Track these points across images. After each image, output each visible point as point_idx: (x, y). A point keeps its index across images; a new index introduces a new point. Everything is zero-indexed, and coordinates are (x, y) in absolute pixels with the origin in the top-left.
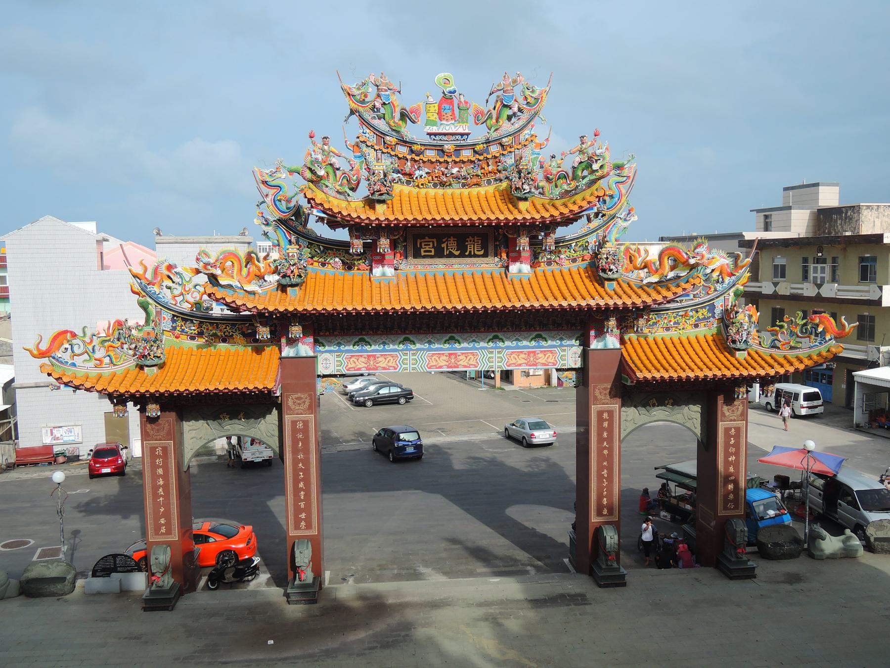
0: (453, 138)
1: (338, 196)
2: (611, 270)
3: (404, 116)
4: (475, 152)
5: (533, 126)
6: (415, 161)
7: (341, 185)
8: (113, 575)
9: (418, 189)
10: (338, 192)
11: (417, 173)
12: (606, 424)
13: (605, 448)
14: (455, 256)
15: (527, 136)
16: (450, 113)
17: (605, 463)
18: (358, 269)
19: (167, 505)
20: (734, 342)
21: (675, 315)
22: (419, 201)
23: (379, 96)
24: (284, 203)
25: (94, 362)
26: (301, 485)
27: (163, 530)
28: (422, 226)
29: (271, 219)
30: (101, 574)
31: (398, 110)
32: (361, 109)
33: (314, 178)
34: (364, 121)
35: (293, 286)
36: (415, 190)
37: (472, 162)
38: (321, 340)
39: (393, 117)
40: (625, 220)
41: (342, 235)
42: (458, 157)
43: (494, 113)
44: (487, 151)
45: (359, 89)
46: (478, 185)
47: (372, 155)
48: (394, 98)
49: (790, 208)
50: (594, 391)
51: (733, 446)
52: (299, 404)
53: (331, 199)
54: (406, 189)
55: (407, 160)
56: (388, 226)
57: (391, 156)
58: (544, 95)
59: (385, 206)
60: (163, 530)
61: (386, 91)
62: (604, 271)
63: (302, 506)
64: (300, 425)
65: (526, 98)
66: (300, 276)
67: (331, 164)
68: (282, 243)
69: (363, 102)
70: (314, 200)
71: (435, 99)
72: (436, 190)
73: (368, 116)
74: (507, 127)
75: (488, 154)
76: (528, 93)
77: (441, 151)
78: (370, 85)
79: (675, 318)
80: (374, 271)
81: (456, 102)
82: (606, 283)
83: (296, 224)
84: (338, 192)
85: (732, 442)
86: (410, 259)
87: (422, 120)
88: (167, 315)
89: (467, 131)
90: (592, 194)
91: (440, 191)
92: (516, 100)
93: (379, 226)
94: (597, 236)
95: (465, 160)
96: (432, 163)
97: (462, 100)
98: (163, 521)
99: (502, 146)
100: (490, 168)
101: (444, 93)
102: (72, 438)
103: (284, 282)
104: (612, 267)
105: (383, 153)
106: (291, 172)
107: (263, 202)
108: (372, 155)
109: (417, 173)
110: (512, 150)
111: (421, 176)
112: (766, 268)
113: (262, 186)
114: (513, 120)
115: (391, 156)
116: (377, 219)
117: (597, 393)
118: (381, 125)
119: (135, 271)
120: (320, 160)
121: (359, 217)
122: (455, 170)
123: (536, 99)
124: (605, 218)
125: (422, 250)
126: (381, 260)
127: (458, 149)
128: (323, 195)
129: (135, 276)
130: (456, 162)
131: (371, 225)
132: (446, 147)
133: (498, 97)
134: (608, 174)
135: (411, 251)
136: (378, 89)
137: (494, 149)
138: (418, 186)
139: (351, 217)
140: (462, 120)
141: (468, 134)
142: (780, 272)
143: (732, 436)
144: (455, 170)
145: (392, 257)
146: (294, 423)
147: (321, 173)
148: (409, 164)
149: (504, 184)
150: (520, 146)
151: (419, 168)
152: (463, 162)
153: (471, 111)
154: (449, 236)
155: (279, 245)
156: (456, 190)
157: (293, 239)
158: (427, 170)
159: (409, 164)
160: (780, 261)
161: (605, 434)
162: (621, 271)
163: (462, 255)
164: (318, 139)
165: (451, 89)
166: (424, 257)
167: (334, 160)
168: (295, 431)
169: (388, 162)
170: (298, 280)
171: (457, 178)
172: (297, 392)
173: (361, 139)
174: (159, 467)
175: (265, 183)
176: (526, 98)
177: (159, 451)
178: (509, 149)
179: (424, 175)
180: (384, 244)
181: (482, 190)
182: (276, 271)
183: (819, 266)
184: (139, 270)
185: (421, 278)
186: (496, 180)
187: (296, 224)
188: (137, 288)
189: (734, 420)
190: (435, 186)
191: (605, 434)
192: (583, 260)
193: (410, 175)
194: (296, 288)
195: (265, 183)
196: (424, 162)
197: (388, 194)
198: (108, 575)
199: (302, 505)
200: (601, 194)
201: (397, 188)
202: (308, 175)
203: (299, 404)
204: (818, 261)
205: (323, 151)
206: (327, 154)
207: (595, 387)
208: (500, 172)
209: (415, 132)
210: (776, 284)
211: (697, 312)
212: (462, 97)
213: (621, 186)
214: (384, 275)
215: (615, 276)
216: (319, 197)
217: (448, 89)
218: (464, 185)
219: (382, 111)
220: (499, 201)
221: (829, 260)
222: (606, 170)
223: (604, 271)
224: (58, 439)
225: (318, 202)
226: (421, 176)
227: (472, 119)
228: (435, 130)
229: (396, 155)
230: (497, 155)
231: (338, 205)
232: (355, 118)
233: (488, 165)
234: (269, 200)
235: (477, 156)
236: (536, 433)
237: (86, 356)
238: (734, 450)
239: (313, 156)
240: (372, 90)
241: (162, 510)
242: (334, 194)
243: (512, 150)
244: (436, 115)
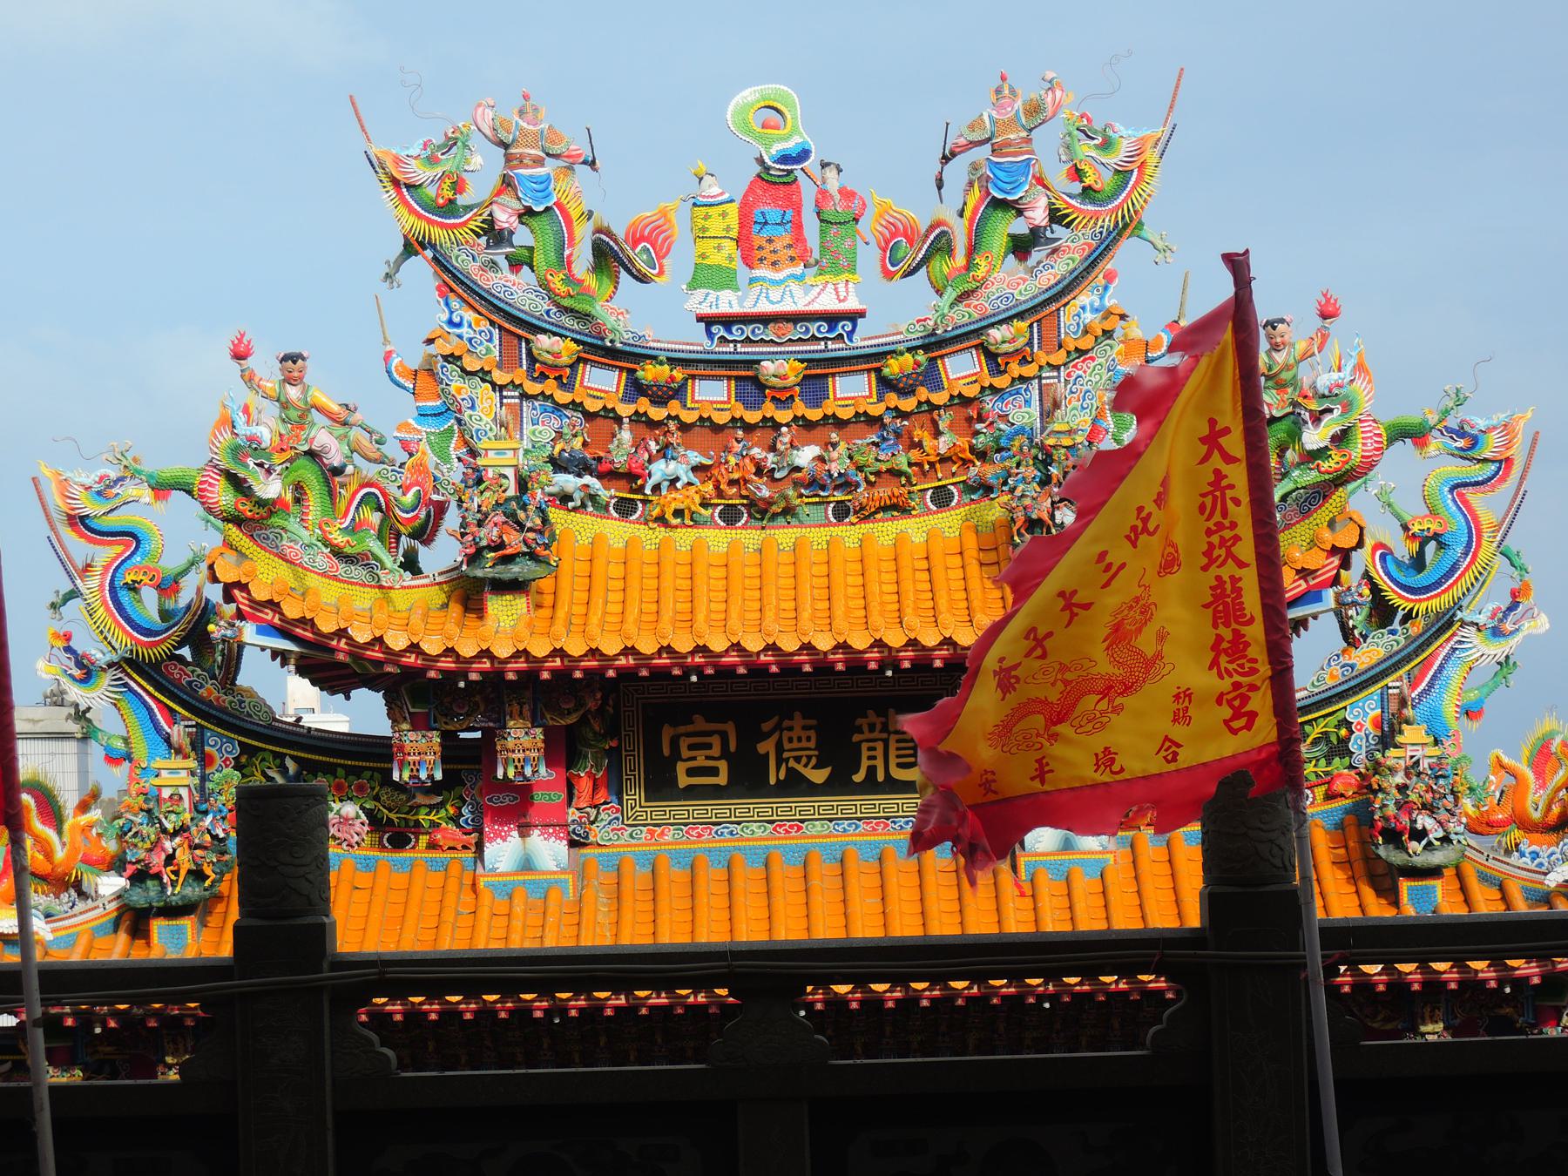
0: (798, 332)
1: (342, 569)
2: (1419, 835)
3: (607, 257)
4: (886, 384)
5: (1110, 277)
6: (653, 424)
7: (354, 528)
9: (661, 532)
10: (337, 553)
11: (660, 470)
14: (812, 789)
15: (1088, 317)
16: (784, 236)
18: (433, 846)
22: (657, 582)
23: (507, 183)
24: (150, 596)
28: (660, 674)
29: (100, 655)
31: (584, 235)
32: (438, 234)
33: (247, 509)
34: (454, 282)
35: (173, 911)
36: (651, 536)
37: (874, 421)
39: (565, 263)
40: (1497, 632)
41: (361, 714)
42: (816, 403)
43: (960, 233)
44: (931, 377)
45: (432, 160)
46: (898, 508)
47: (484, 408)
53: (312, 581)
54: (616, 531)
55: (618, 420)
56: (562, 675)
57: (558, 407)
58: (1151, 157)
59: (520, 603)
61: (539, 162)
62: (1393, 837)
65: (1077, 174)
66: (197, 875)
67: (311, 454)
68: (140, 750)
69: (449, 208)
70: (244, 587)
71: (730, 183)
72: (732, 534)
74: (1014, 283)
75: (937, 386)
76: (1085, 150)
77: (751, 384)
78: (477, 141)
80: (490, 850)
81: (808, 193)
82: (1405, 886)
83: (193, 675)
84: (337, 553)
86: (634, 796)
87: (678, 264)
89: (852, 304)
90: (1313, 544)
91: (748, 537)
92: (1040, 181)
93: (494, 678)
94: (1384, 699)
95: (846, 414)
96: (717, 428)
97: (833, 183)
99: (991, 356)
100: (944, 444)
101: (761, 161)
103: (139, 898)
104: (1424, 821)
105: (525, 396)
106: (162, 489)
107: (73, 594)
108: (484, 408)
109: (660, 470)
110: (1030, 370)
111: (674, 482)
113: (68, 534)
114: (1037, 255)
115: (558, 407)
116: (486, 653)
118: (520, 291)
120: (266, 443)
121: (414, 648)
122: (805, 456)
124: (1414, 629)
125: (681, 768)
126: (516, 807)
127: (816, 377)
128: (283, 570)
130: (808, 425)
131: (464, 674)
132: (769, 367)
133: (975, 167)
134: (1368, 466)
135: (635, 766)
136: (508, 158)
137: (961, 369)
138: (661, 520)
139: (388, 651)
140: (834, 262)
141: (854, 316)
144: (805, 456)
145: (559, 796)
147: (270, 488)
148: (626, 435)
149: (993, 511)
150: (1059, 357)
151: (664, 452)
152: (840, 424)
153: (869, 226)
154: (784, 710)
155: (128, 757)
156: (813, 534)
157: (178, 733)
158: (695, 458)
159: (626, 435)
162: (1444, 836)
163: (839, 784)
164: (265, 365)
165: (791, 145)
166: (692, 793)
167: (323, 437)
169: (545, 432)
170: (193, 892)
171: (814, 483)
173: (442, 348)
175: (79, 522)
176: (1077, 174)
178: (1016, 369)
179: (685, 476)
180: (522, 746)
181: (914, 529)
182: (116, 864)
185: (674, 873)
186: (968, 488)
187: (193, 675)
190: (730, 516)
192: (1330, 796)
193: (631, 478)
194: (187, 923)
195: (79, 522)
196: (684, 427)
197: (532, 556)
200: (1346, 539)
201: (577, 530)
202: (224, 496)
205: (285, 405)
206: (297, 416)
208: (982, 455)
209: (656, 314)
212: (831, 173)
213: (1475, 498)
214: (527, 866)
215: (1437, 858)
216: (267, 575)
217: (777, 148)
218: (842, 512)
219: (522, 237)
220: (973, 568)
222: (1356, 452)
223: (1393, 837)
225: (260, 594)
226: (674, 482)
227: (869, 257)
228: (727, 302)
229: (575, 406)
230: (972, 391)
231: (346, 607)
232: (420, 269)
233: (937, 434)
234: (91, 585)
235: (893, 399)
239: (243, 429)
240: (483, 166)
242: (323, 560)
243: (1030, 370)
244: (730, 247)
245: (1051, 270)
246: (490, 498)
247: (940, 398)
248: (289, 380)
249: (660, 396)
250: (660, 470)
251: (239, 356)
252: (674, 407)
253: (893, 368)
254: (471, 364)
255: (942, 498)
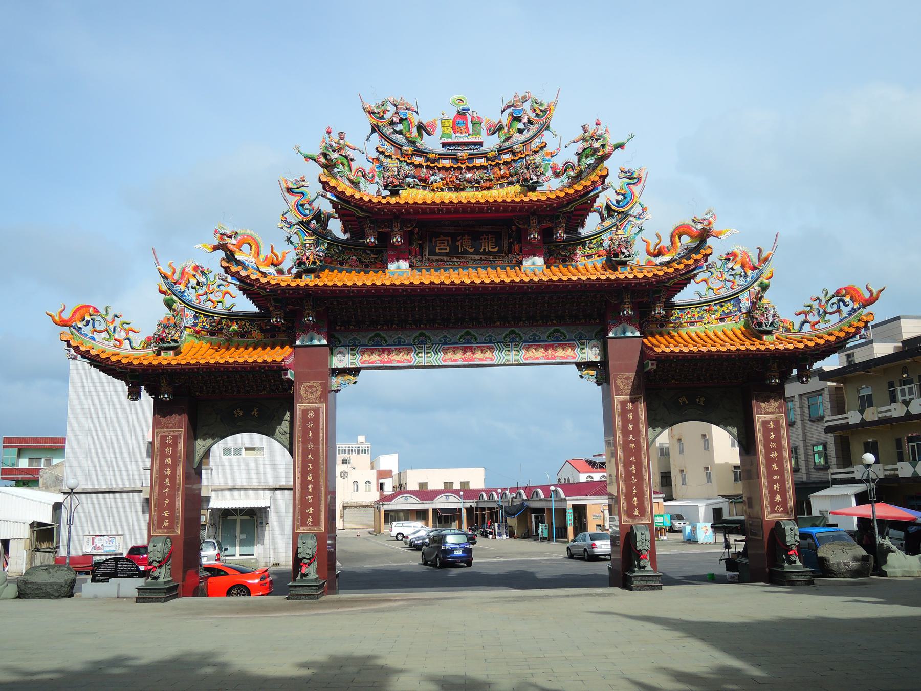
2: (624, 253)
8: (112, 580)
12: (630, 416)
13: (631, 441)
17: (632, 459)
19: (172, 497)
20: (760, 324)
21: (698, 309)
25: (113, 342)
26: (310, 477)
27: (166, 524)
30: (101, 578)
34: (383, 136)
38: (336, 335)
40: (639, 218)
46: (489, 188)
48: (410, 114)
49: (871, 342)
50: (615, 380)
51: (774, 441)
52: (311, 393)
60: (166, 524)
63: (310, 500)
64: (311, 414)
65: (535, 110)
71: (451, 114)
73: (388, 131)
76: (536, 106)
77: (456, 159)
79: (698, 312)
85: (772, 436)
87: (438, 131)
88: (190, 313)
97: (475, 115)
98: (166, 514)
100: (502, 172)
102: (112, 548)
104: (624, 250)
109: (432, 178)
112: (850, 397)
113: (288, 196)
117: (619, 382)
118: (399, 138)
119: (163, 270)
122: (469, 175)
123: (544, 111)
129: (165, 277)
134: (609, 155)
138: (433, 190)
142: (866, 402)
143: (771, 430)
144: (469, 175)
146: (305, 412)
158: (441, 175)
160: (865, 391)
161: (630, 427)
168: (305, 420)
172: (309, 380)
174: (168, 456)
175: (289, 190)
177: (169, 440)
183: (906, 387)
184: (169, 273)
188: (164, 288)
189: (772, 413)
191: (630, 427)
192: (599, 256)
193: (424, 180)
195: (289, 190)
198: (107, 581)
199: (310, 499)
200: (604, 173)
203: (311, 393)
204: (905, 382)
207: (616, 376)
209: (432, 143)
210: (862, 412)
211: (722, 306)
214: (398, 268)
221: (916, 379)
222: (606, 150)
224: (98, 548)
227: (484, 132)
233: (500, 170)
236: (597, 543)
237: (105, 334)
238: (775, 445)
241: (167, 502)
245: (527, 135)
246: (390, 173)
247: (501, 162)
248: (342, 138)
249: (433, 161)
250: (432, 178)
251: (329, 132)
252: (436, 164)
253: (490, 155)
254: (387, 154)
255: (502, 185)
